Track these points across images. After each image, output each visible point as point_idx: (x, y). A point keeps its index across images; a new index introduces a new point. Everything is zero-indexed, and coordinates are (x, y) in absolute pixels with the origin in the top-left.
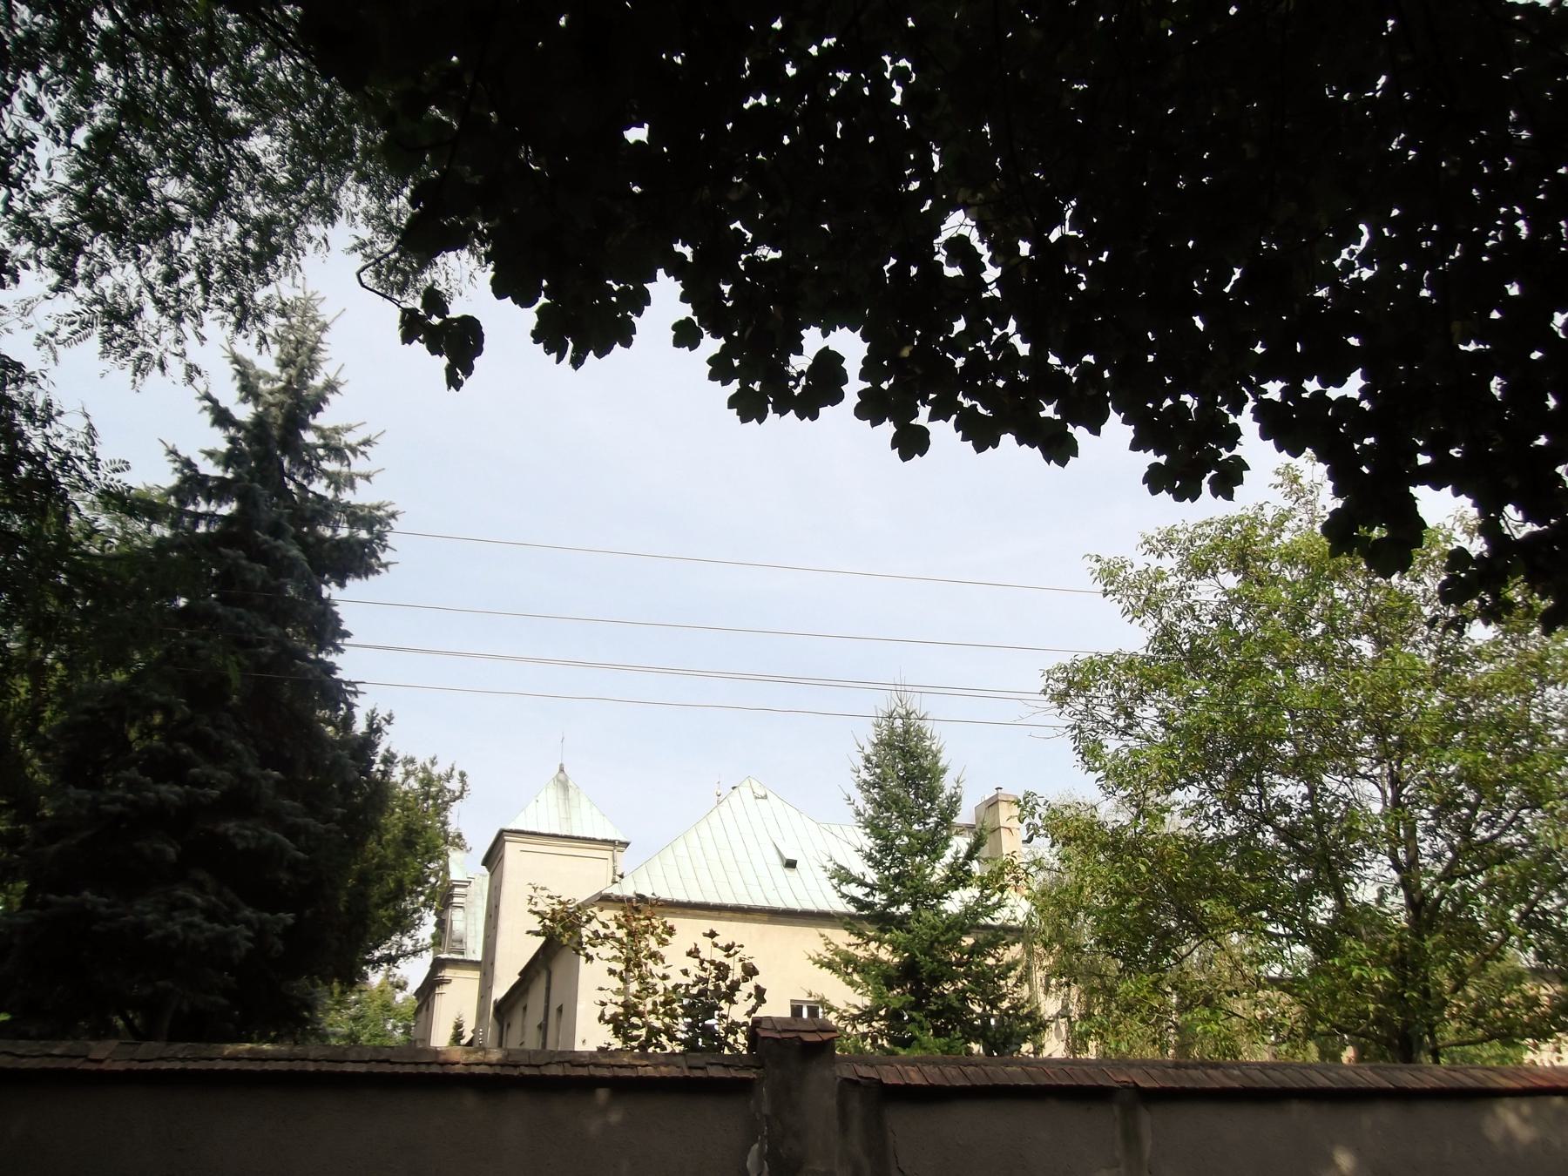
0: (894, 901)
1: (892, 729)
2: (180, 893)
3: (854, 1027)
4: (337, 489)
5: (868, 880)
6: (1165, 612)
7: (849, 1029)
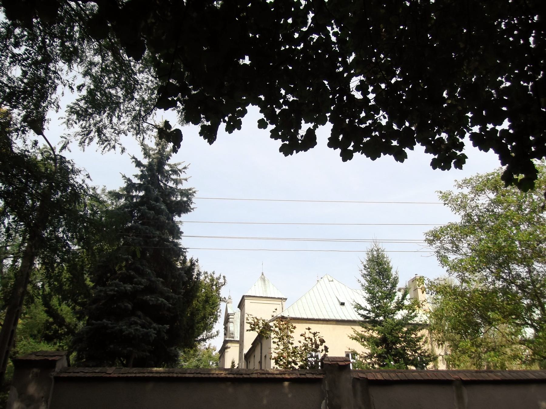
0: (377, 315)
1: (373, 255)
2: (133, 319)
3: (366, 360)
4: (177, 184)
5: (368, 309)
6: (467, 208)
7: (364, 361)
